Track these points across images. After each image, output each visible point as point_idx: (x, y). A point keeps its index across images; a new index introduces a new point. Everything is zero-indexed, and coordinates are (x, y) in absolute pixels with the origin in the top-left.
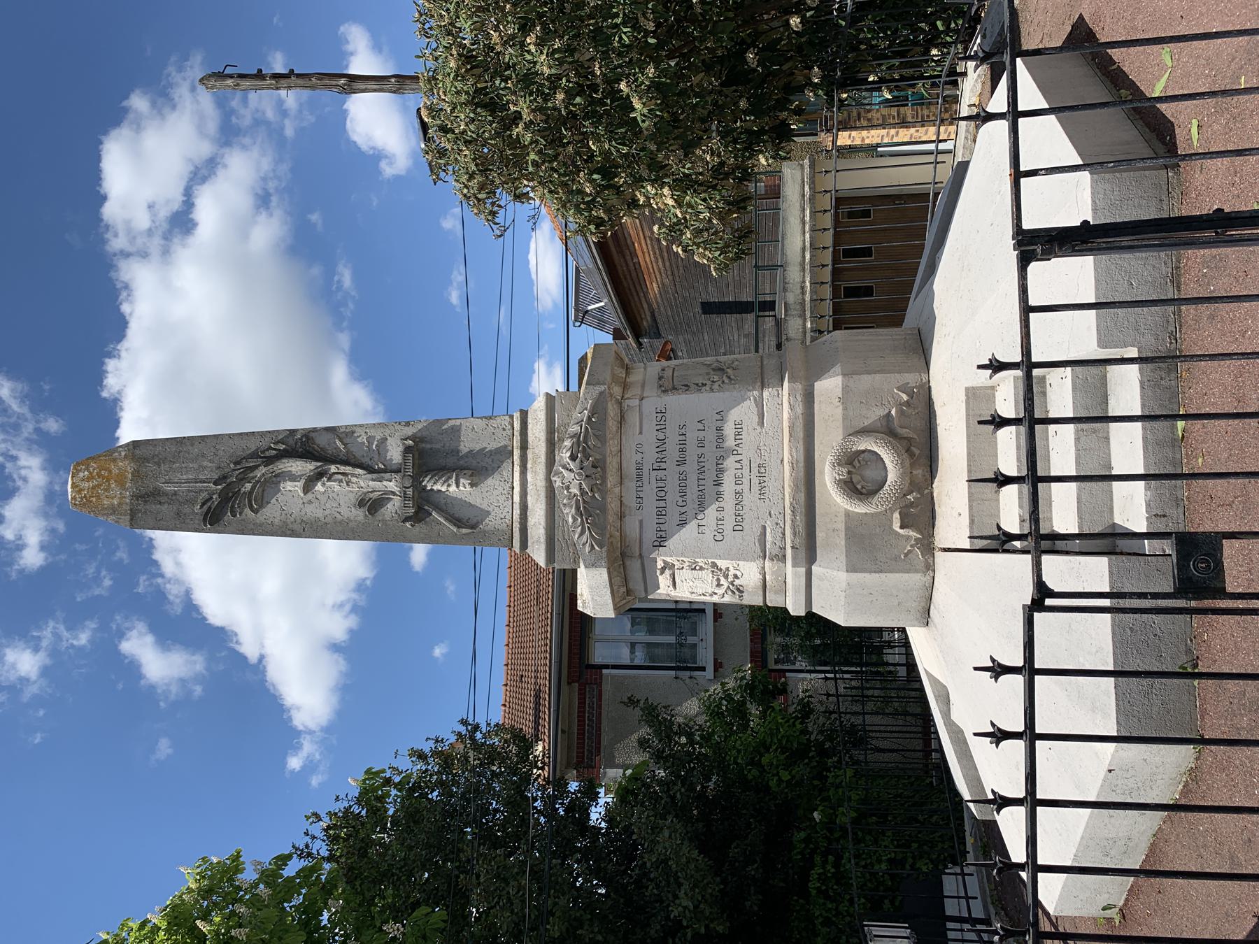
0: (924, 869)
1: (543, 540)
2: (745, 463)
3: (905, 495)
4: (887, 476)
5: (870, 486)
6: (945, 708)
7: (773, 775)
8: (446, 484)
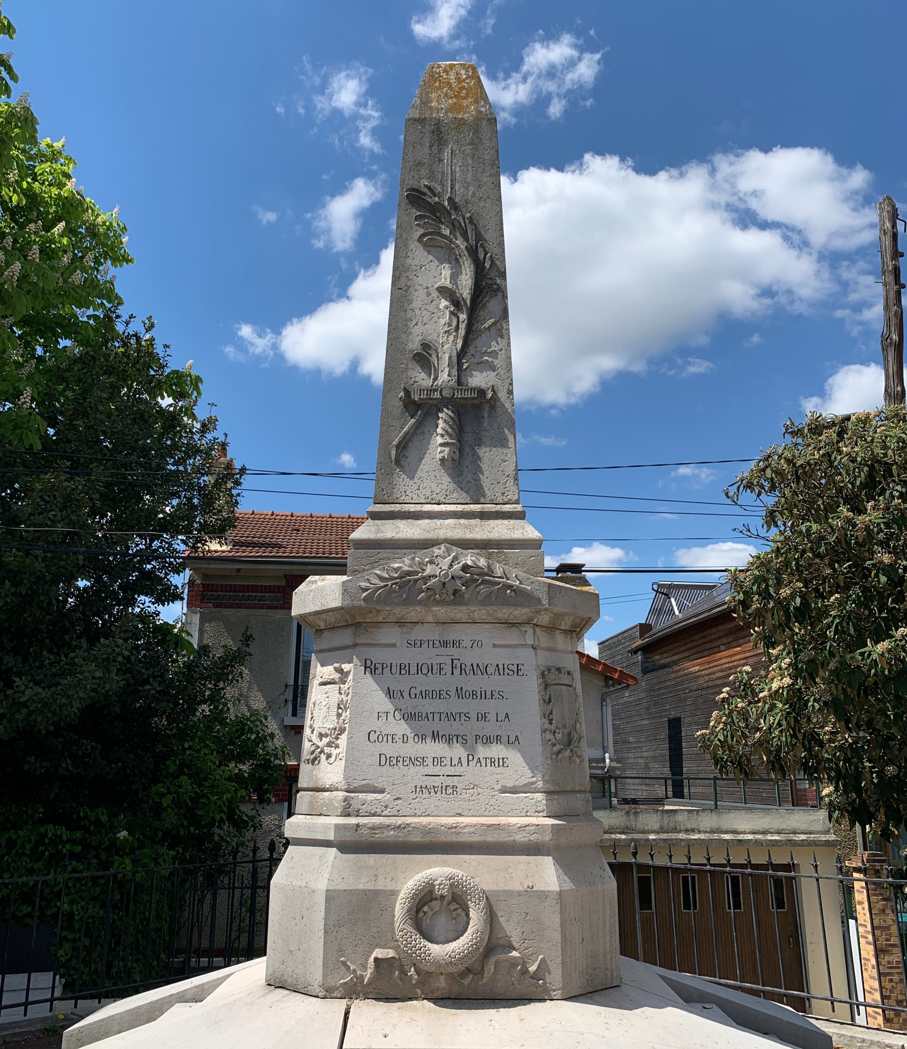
0: (61, 952)
1: (380, 536)
2: (458, 770)
3: (415, 965)
4: (437, 943)
5: (426, 922)
6: (189, 996)
7: (168, 788)
8: (444, 433)
